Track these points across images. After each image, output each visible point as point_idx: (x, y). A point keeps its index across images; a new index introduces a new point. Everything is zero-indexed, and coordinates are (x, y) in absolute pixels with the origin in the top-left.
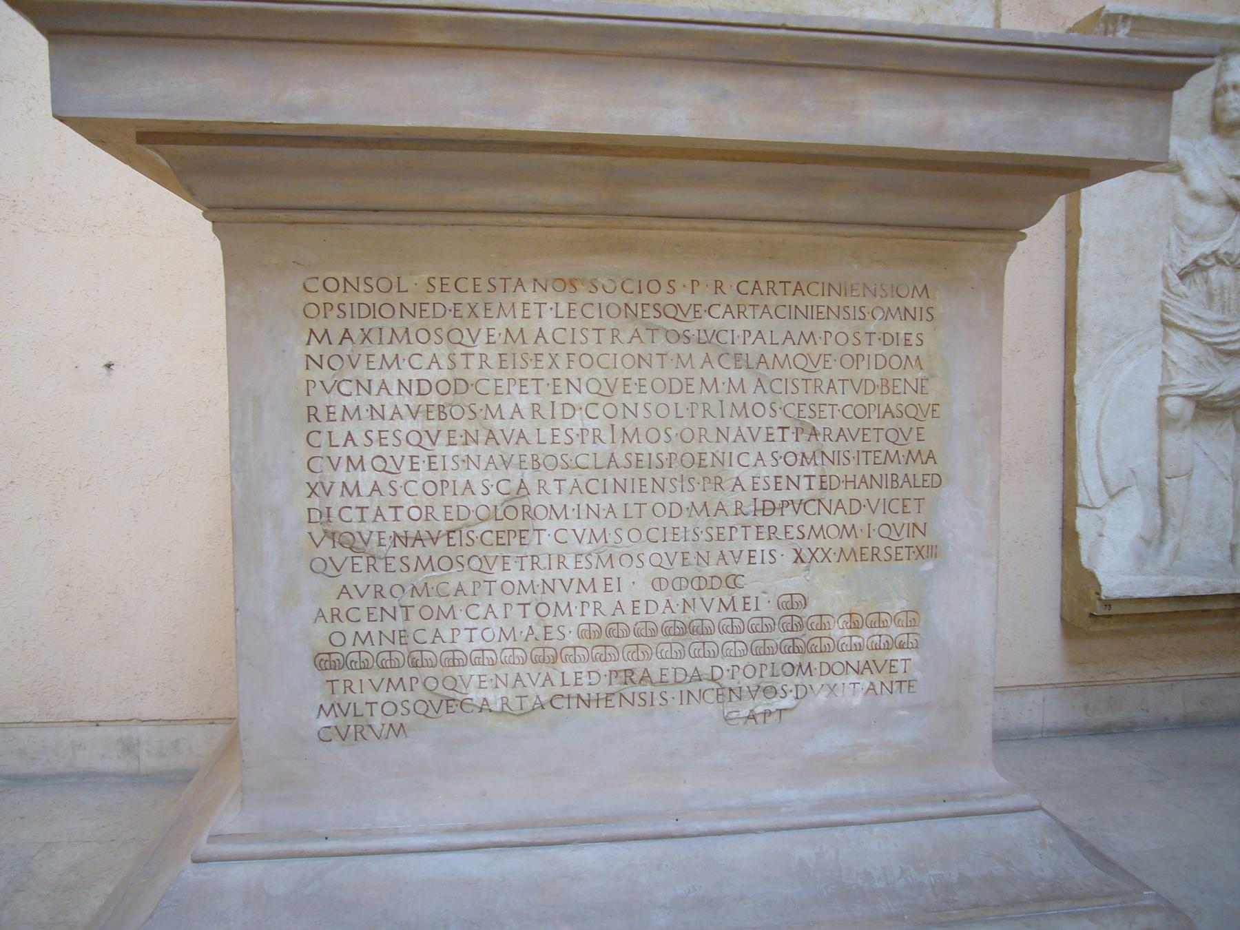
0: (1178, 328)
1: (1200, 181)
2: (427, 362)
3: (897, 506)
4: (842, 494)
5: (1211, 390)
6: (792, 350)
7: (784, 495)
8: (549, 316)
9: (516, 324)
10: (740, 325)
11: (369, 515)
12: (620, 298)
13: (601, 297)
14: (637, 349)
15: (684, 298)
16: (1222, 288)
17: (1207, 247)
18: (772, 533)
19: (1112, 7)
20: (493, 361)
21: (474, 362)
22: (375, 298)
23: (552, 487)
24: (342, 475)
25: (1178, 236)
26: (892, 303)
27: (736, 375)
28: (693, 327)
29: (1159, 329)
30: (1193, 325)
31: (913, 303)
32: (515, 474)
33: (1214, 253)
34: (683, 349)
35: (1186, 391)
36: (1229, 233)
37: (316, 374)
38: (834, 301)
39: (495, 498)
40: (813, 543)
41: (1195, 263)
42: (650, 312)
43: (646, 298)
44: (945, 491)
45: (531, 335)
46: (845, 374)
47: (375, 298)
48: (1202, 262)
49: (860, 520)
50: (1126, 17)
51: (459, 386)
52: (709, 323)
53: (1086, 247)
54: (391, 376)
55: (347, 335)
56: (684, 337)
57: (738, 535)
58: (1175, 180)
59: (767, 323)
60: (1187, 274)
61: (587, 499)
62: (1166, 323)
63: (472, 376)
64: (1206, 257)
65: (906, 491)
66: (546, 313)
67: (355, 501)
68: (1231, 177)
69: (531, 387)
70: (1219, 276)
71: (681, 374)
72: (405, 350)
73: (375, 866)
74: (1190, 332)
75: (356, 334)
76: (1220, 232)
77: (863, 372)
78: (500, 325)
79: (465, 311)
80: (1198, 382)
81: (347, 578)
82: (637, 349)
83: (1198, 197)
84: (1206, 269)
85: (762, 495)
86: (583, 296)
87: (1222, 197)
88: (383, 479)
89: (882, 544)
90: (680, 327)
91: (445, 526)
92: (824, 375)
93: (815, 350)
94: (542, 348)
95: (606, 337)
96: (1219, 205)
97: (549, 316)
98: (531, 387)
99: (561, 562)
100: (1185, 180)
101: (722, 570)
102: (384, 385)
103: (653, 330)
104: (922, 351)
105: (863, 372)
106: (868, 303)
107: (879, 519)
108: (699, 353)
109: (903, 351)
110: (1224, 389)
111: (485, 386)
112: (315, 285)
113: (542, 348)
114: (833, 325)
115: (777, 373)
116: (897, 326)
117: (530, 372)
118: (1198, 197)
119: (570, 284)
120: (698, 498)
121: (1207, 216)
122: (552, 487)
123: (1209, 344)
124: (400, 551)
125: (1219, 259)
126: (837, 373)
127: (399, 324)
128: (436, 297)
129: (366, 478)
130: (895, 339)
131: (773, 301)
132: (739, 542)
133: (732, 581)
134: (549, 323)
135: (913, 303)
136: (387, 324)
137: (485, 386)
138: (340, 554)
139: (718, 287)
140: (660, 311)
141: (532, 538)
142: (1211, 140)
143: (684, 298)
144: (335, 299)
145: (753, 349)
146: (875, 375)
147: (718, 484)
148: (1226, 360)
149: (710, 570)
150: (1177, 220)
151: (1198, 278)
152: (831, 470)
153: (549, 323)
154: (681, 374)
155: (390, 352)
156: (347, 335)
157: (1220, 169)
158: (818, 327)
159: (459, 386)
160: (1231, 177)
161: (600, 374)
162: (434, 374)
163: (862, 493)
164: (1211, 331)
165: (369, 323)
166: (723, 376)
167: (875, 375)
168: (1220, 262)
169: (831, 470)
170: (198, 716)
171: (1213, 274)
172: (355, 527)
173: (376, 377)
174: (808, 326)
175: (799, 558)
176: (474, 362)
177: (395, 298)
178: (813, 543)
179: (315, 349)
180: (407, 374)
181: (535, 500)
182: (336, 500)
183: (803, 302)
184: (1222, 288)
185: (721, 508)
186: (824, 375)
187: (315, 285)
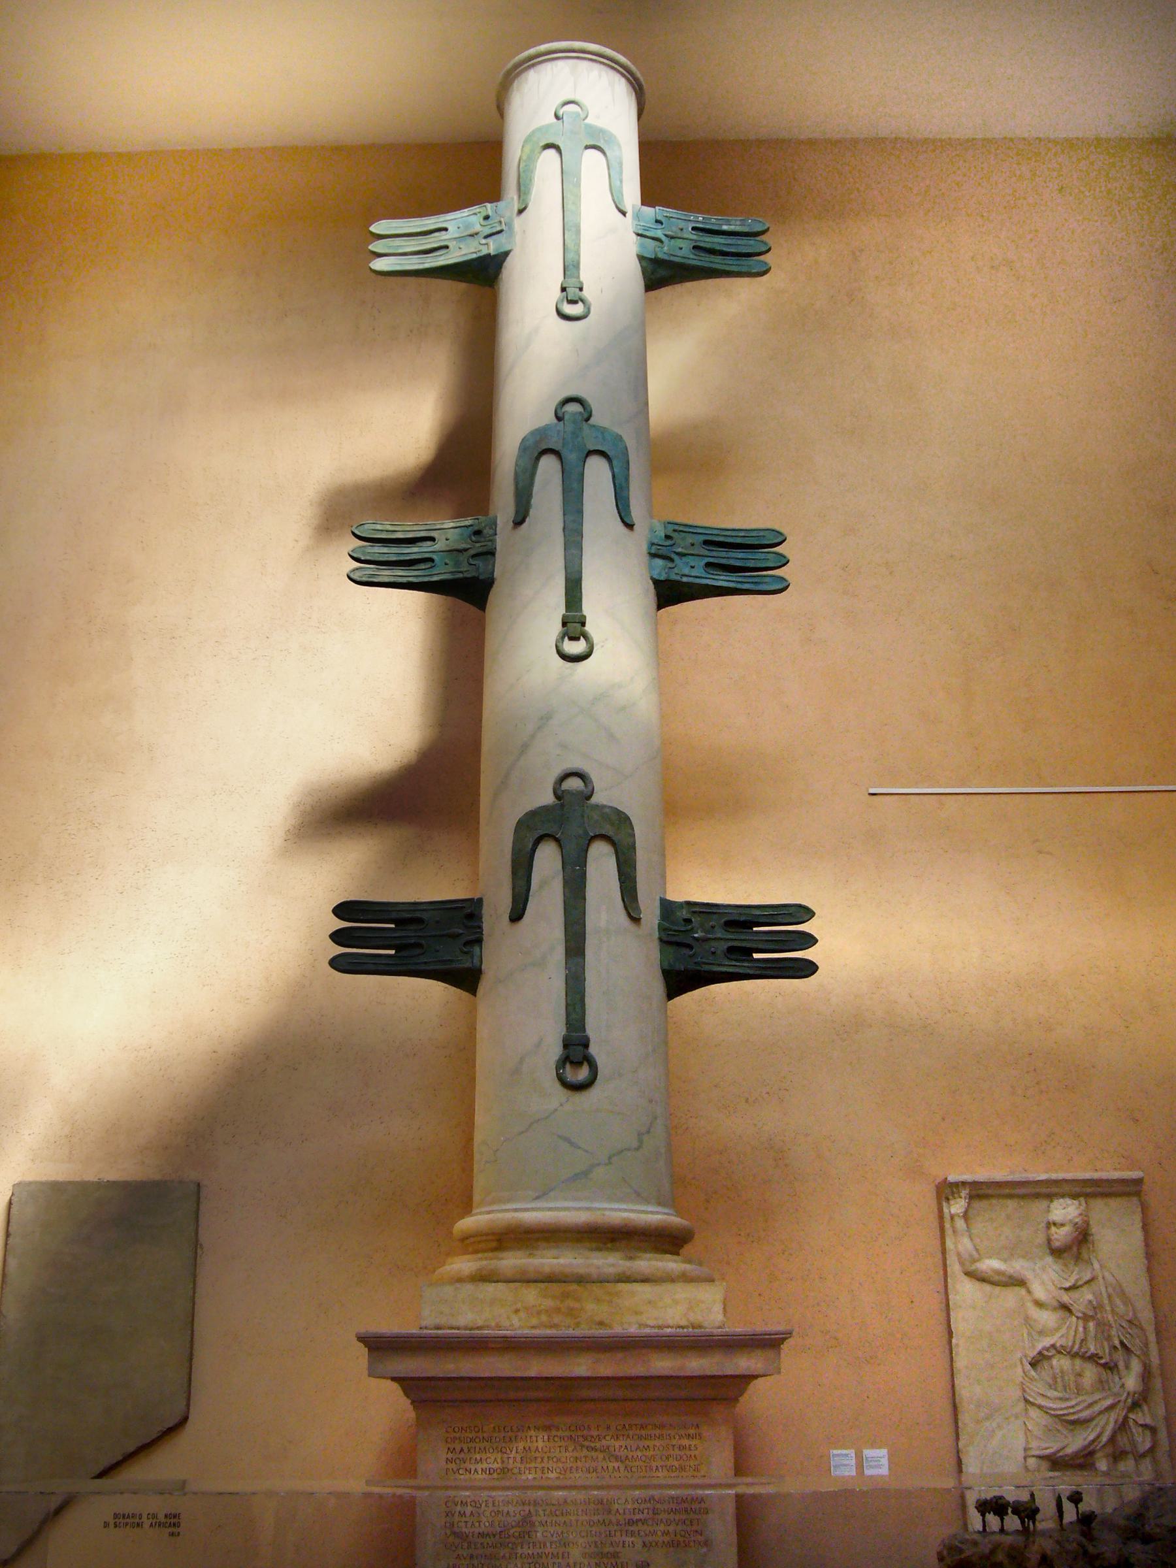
0: (1033, 1404)
1: (1040, 1293)
2: (493, 1461)
3: (688, 1522)
4: (663, 1516)
5: (1059, 1451)
6: (639, 1454)
7: (638, 1517)
8: (540, 1440)
9: (529, 1444)
10: (617, 1444)
11: (469, 1524)
12: (568, 1433)
13: (560, 1433)
14: (576, 1454)
15: (595, 1433)
16: (1062, 1372)
17: (1047, 1342)
18: (632, 1534)
19: (952, 1178)
20: (519, 1459)
21: (511, 1461)
22: (473, 1435)
23: (541, 1513)
24: (459, 1508)
25: (1029, 1334)
26: (682, 1432)
27: (616, 1465)
28: (598, 1445)
29: (1022, 1404)
30: (1040, 1401)
31: (692, 1431)
32: (527, 1508)
33: (1053, 1346)
34: (593, 1454)
35: (1037, 1453)
36: (1063, 1331)
37: (450, 1466)
38: (657, 1432)
39: (518, 1517)
40: (650, 1538)
41: (1040, 1353)
42: (581, 1439)
43: (579, 1433)
44: (710, 1516)
45: (533, 1449)
46: (662, 1463)
47: (473, 1435)
48: (1046, 1353)
49: (671, 1528)
50: (964, 1183)
51: (504, 1471)
52: (604, 1442)
53: (957, 1345)
54: (479, 1466)
55: (462, 1450)
56: (594, 1449)
57: (618, 1534)
58: (1023, 1291)
59: (629, 1442)
60: (1038, 1362)
61: (555, 1518)
62: (1026, 1400)
63: (510, 1466)
64: (1047, 1349)
65: (692, 1515)
66: (540, 1441)
67: (464, 1519)
68: (1061, 1288)
69: (533, 1471)
70: (1061, 1363)
71: (594, 1464)
72: (484, 1456)
73: (458, 524)
74: (1040, 1407)
75: (466, 1450)
76: (1057, 1329)
77: (671, 1462)
78: (521, 1445)
79: (507, 1439)
80: (1047, 1445)
81: (460, 1552)
82: (576, 1454)
83: (1039, 1304)
84: (1049, 1358)
85: (628, 1517)
86: (554, 1433)
87: (1055, 1304)
88: (474, 1510)
89: (681, 1539)
90: (593, 1445)
91: (499, 1530)
92: (654, 1464)
93: (650, 1453)
94: (538, 1455)
95: (563, 1450)
96: (1055, 1309)
97: (540, 1440)
98: (533, 1471)
99: (545, 1545)
100: (1029, 1292)
101: (611, 1550)
102: (476, 1470)
103: (582, 1446)
104: (697, 1452)
105: (671, 1462)
106: (672, 1433)
107: (680, 1528)
108: (601, 1456)
109: (688, 1453)
110: (1069, 1450)
111: (515, 1471)
112: (450, 1430)
113: (538, 1455)
114: (657, 1443)
115: (635, 1464)
116: (685, 1442)
117: (533, 1465)
118: (1039, 1304)
119: (547, 1428)
120: (600, 1518)
121: (1047, 1318)
122: (541, 1513)
123: (1057, 1416)
124: (481, 1540)
125: (1058, 1350)
126: (659, 1463)
127: (482, 1445)
128: (496, 1435)
129: (469, 1509)
130: (684, 1448)
131: (631, 1433)
132: (618, 1538)
133: (615, 1555)
134: (540, 1444)
135: (692, 1431)
136: (478, 1446)
137: (515, 1471)
138: (457, 1541)
139: (608, 1428)
140: (585, 1439)
141: (533, 1534)
142: (1049, 1259)
143: (595, 1433)
144: (458, 1435)
145: (623, 1453)
146: (676, 1464)
147: (610, 1512)
148: (1071, 1427)
149: (606, 1550)
150: (1027, 1320)
151: (1046, 1364)
152: (658, 1506)
153: (540, 1444)
154: (594, 1464)
155: (478, 1456)
156: (462, 1450)
157: (1053, 1282)
158: (650, 1443)
159: (504, 1471)
160: (1061, 1288)
161: (560, 1465)
162: (495, 1466)
163: (671, 1516)
164: (1055, 1406)
165: (472, 1445)
166: (611, 1465)
167: (676, 1464)
168: (1059, 1352)
169: (658, 1506)
170: (588, 1285)
171: (1054, 1362)
172: (464, 1530)
173: (473, 1467)
174: (647, 1443)
175: (644, 1545)
176: (511, 1461)
177: (480, 1435)
178: (650, 1538)
179: (450, 1455)
180: (485, 1466)
181: (534, 1518)
182: (456, 1518)
183: (643, 1432)
184: (1062, 1372)
185: (610, 1522)
186: (654, 1464)
187: (450, 1430)
